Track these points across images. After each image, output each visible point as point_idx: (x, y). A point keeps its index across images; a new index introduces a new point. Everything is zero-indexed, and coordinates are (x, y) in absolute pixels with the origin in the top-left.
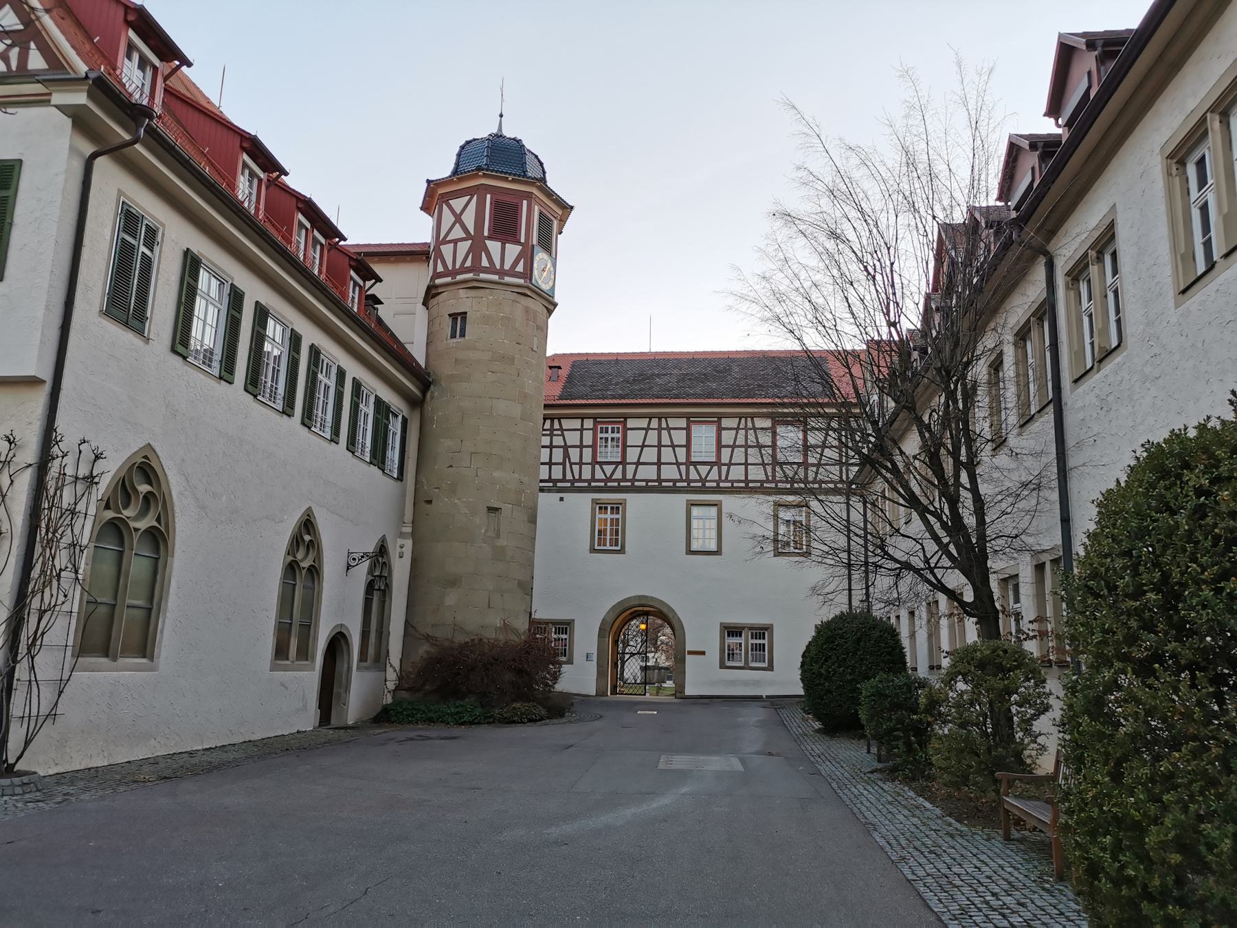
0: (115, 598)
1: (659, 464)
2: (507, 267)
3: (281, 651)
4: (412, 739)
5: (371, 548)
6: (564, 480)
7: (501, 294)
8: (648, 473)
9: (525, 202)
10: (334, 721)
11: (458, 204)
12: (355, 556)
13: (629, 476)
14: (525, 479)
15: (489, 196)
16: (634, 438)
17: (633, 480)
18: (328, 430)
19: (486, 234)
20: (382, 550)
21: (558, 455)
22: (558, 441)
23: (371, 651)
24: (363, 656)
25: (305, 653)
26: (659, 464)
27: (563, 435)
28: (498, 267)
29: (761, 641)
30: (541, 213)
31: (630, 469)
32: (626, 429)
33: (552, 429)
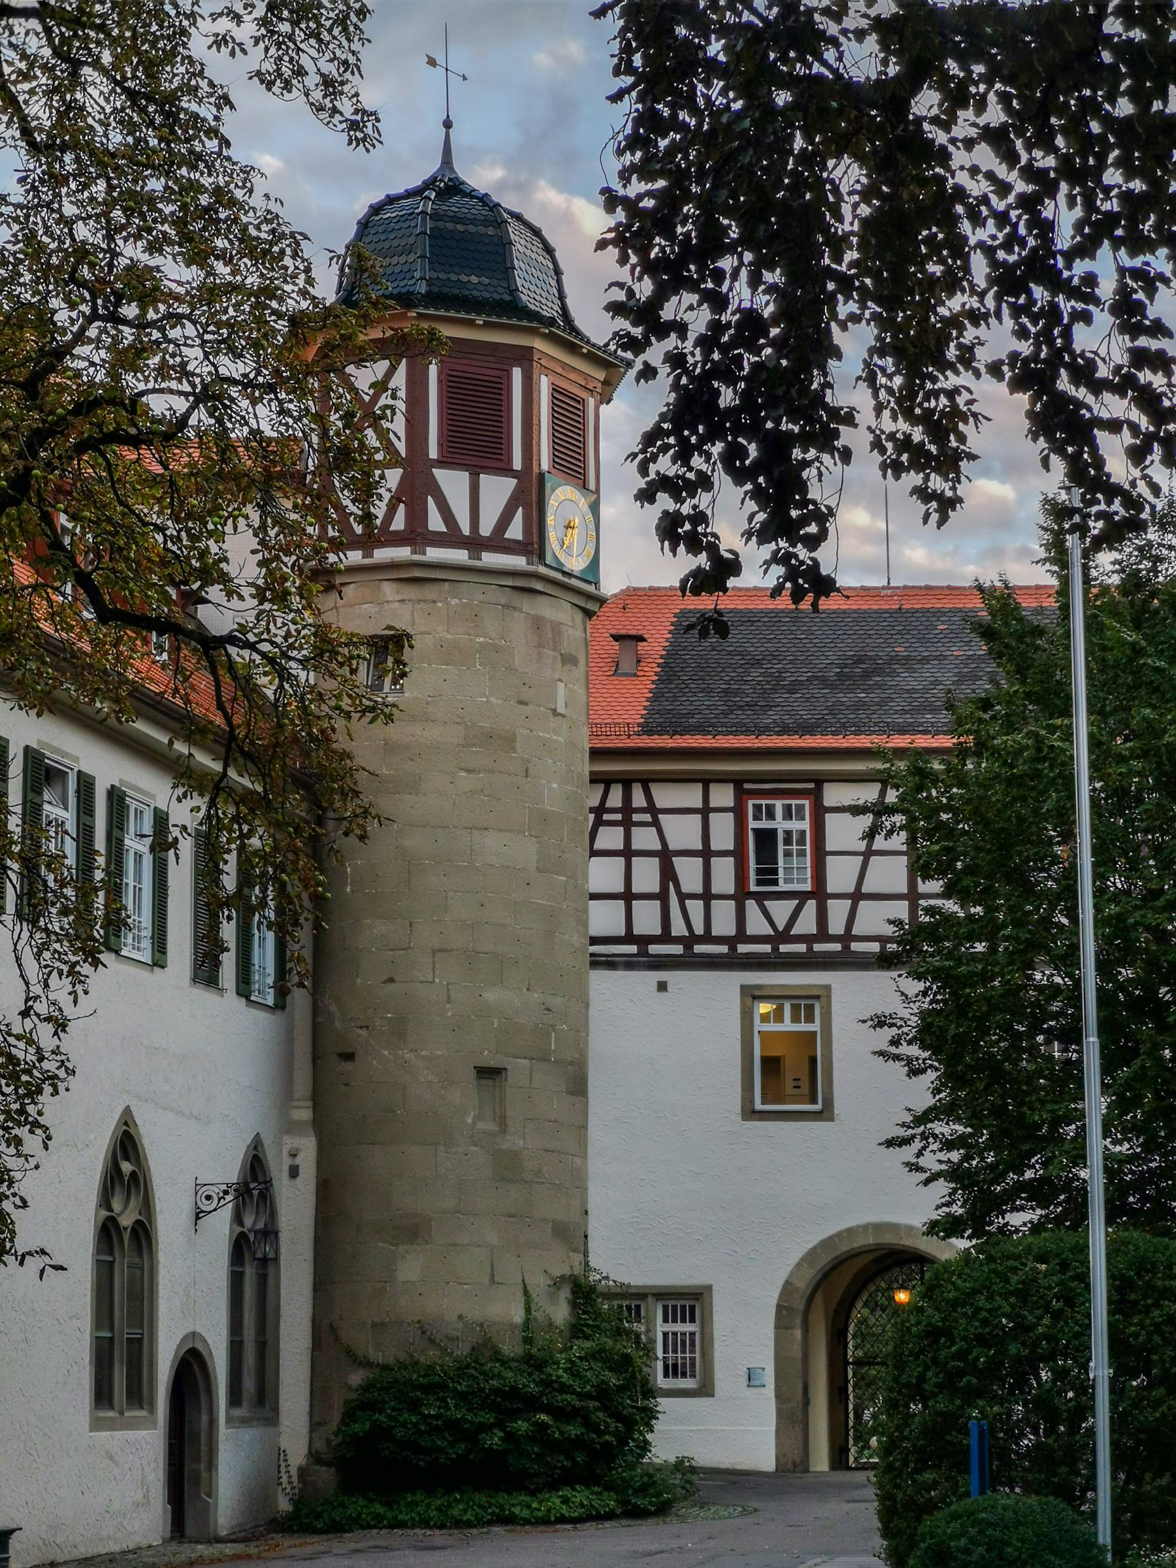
2: (486, 530)
3: (102, 1395)
4: (358, 1551)
5: (230, 1170)
6: (666, 937)
7: (477, 594)
9: (517, 373)
10: (190, 1530)
12: (214, 1191)
13: (836, 926)
14: (556, 1002)
15: (433, 370)
17: (847, 937)
18: (146, 944)
19: (433, 454)
20: (255, 1164)
21: (647, 875)
22: (644, 838)
23: (249, 1384)
24: (235, 1398)
25: (138, 1395)
27: (656, 823)
28: (466, 530)
29: (671, 1327)
30: (557, 392)
31: (838, 912)
32: (819, 813)
33: (627, 809)
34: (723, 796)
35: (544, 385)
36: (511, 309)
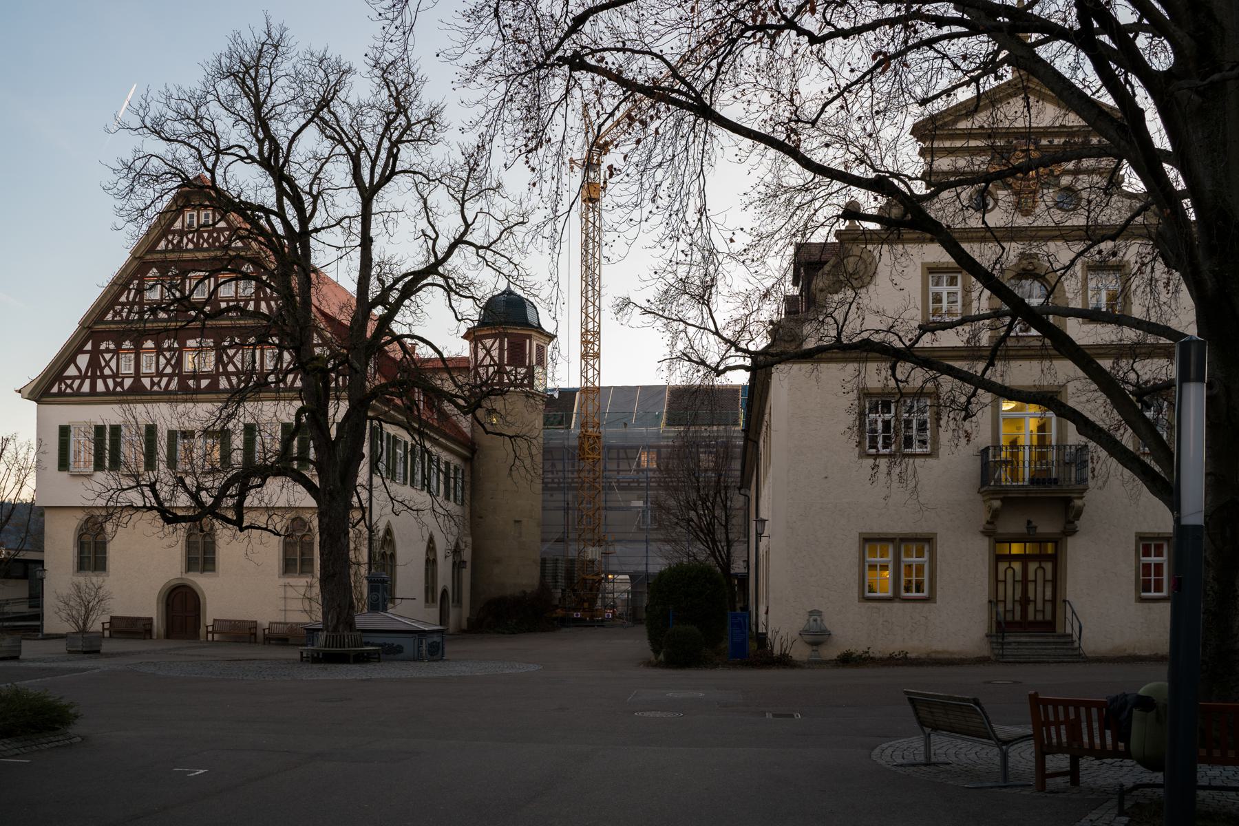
0: (1051, 792)
3: (427, 601)
11: (488, 342)
25: (434, 600)
36: (526, 324)
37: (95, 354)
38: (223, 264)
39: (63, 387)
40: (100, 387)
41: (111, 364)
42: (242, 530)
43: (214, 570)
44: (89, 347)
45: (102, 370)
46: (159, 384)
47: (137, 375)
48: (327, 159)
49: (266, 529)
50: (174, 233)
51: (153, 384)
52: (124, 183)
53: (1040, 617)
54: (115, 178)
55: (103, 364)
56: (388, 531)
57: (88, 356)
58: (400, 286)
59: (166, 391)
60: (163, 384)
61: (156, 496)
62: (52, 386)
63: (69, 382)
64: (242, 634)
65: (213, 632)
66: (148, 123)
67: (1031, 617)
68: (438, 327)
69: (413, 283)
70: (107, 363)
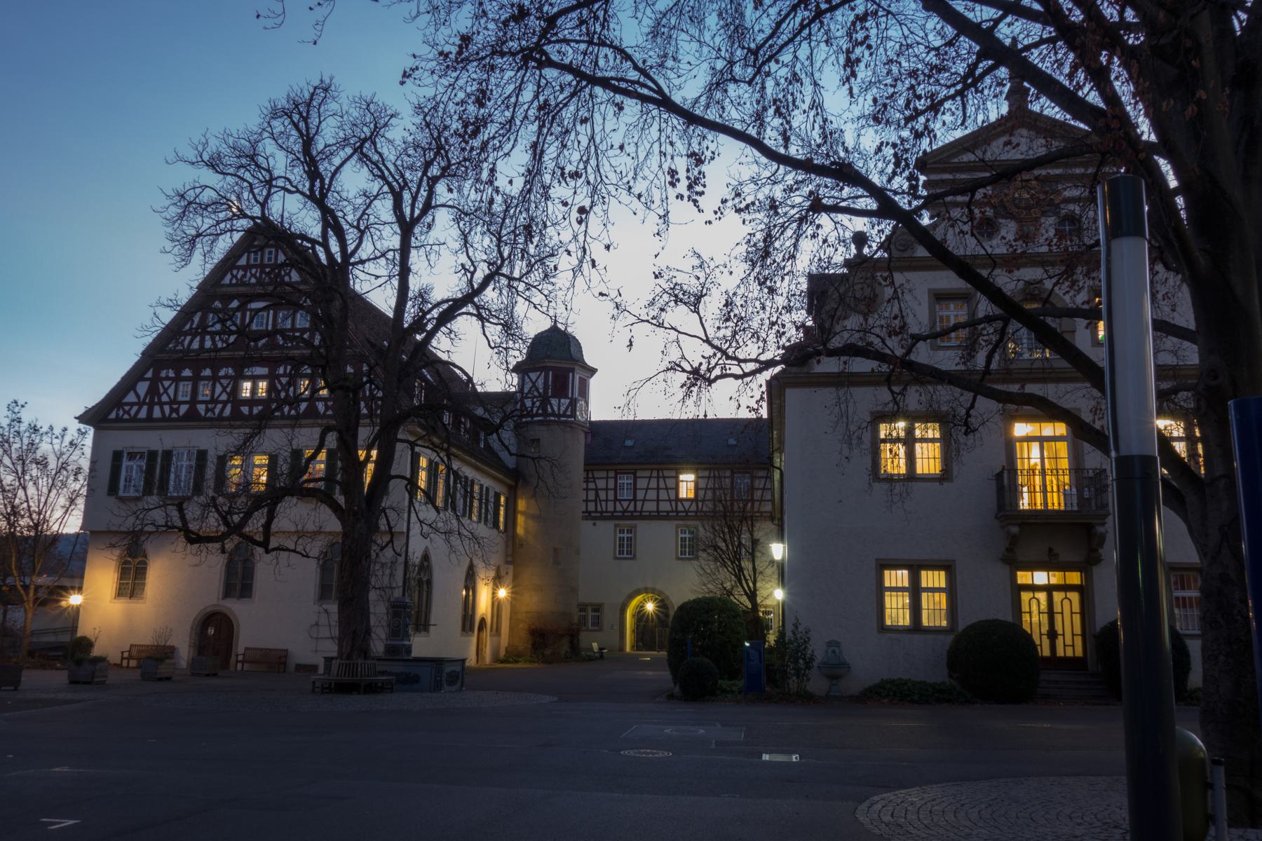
1: (658, 500)
3: (464, 629)
8: (650, 507)
13: (639, 509)
16: (642, 483)
26: (658, 500)
31: (639, 504)
32: (635, 479)
34: (612, 474)
35: (577, 377)
37: (155, 381)
38: (282, 299)
39: (121, 412)
40: (157, 413)
41: (169, 390)
42: (267, 552)
43: (250, 596)
44: (149, 374)
45: (160, 396)
46: (212, 410)
47: (194, 401)
48: (376, 197)
49: (294, 551)
50: (239, 268)
51: (207, 410)
52: (174, 211)
53: (1069, 653)
54: (168, 202)
55: (162, 390)
56: (426, 557)
57: (148, 383)
58: (435, 313)
59: (220, 418)
60: (217, 411)
61: (183, 517)
62: (110, 413)
63: (127, 408)
64: (274, 662)
65: (243, 662)
66: (206, 157)
67: (1060, 653)
68: (479, 358)
69: (452, 310)
70: (166, 390)
